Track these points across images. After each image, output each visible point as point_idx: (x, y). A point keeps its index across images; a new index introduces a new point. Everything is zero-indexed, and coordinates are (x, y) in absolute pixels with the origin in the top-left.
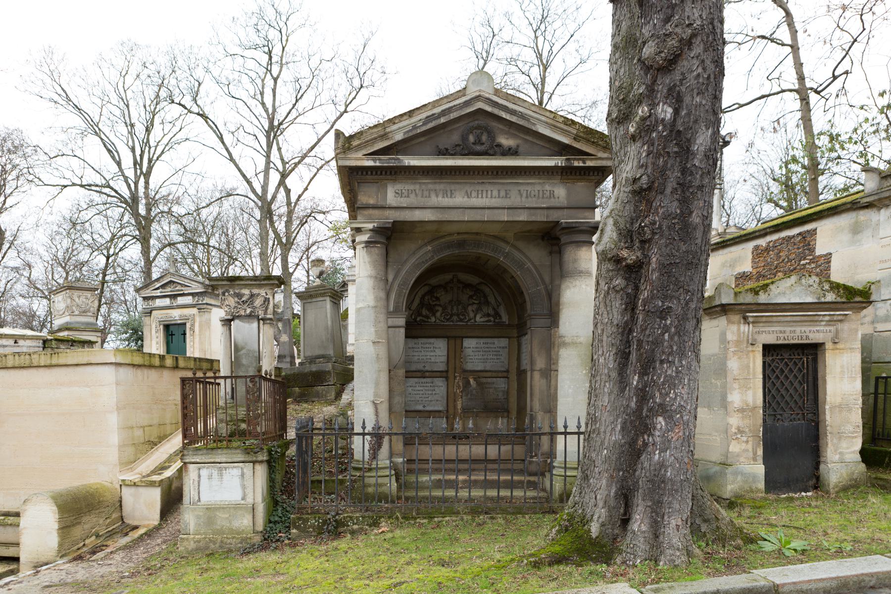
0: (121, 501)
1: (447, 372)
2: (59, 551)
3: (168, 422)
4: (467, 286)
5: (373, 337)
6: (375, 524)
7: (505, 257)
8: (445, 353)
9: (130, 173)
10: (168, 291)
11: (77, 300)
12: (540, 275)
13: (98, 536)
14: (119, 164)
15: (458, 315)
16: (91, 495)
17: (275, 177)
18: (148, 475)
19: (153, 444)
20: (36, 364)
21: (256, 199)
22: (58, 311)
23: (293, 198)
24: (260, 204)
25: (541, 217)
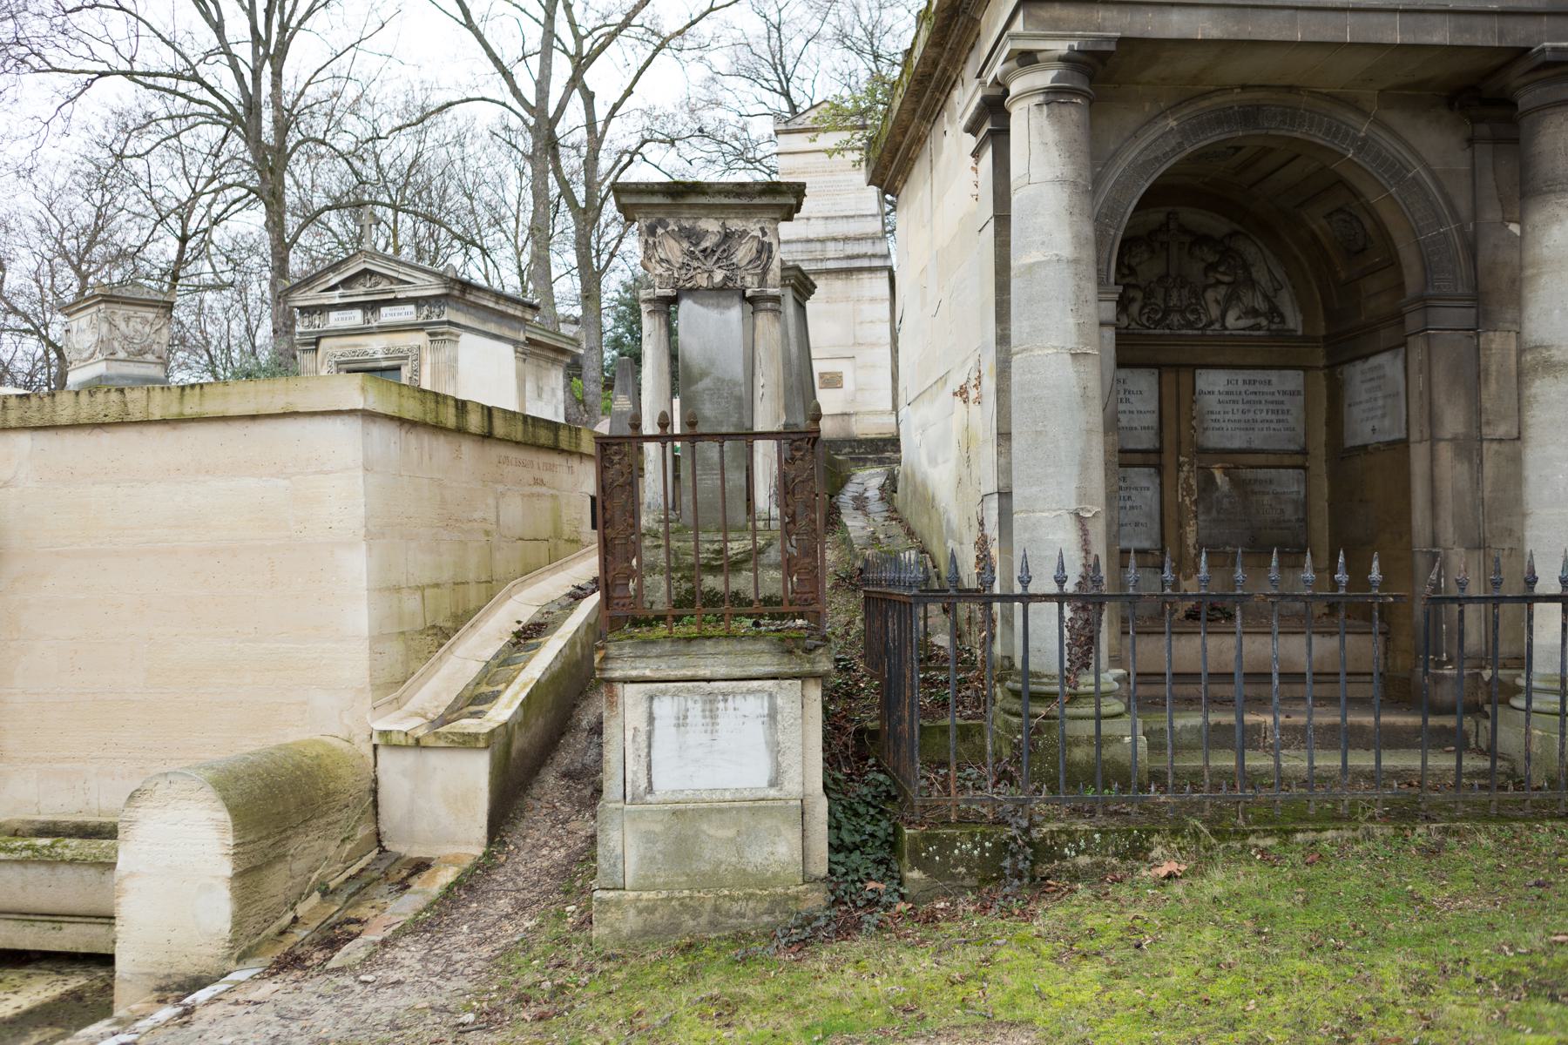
0: (375, 792)
1: (1159, 451)
2: (234, 941)
3: (471, 576)
4: (1202, 239)
5: (1072, 341)
6: (1138, 852)
7: (1360, 150)
8: (1154, 405)
9: (244, 52)
10: (359, 292)
11: (122, 326)
12: (1445, 196)
13: (326, 893)
14: (218, 28)
15: (1182, 312)
16: (308, 774)
17: (562, 68)
18: (444, 720)
19: (442, 633)
20: (138, 416)
22: (79, 352)
23: (601, 113)
24: (532, 121)
25: (1484, 35)
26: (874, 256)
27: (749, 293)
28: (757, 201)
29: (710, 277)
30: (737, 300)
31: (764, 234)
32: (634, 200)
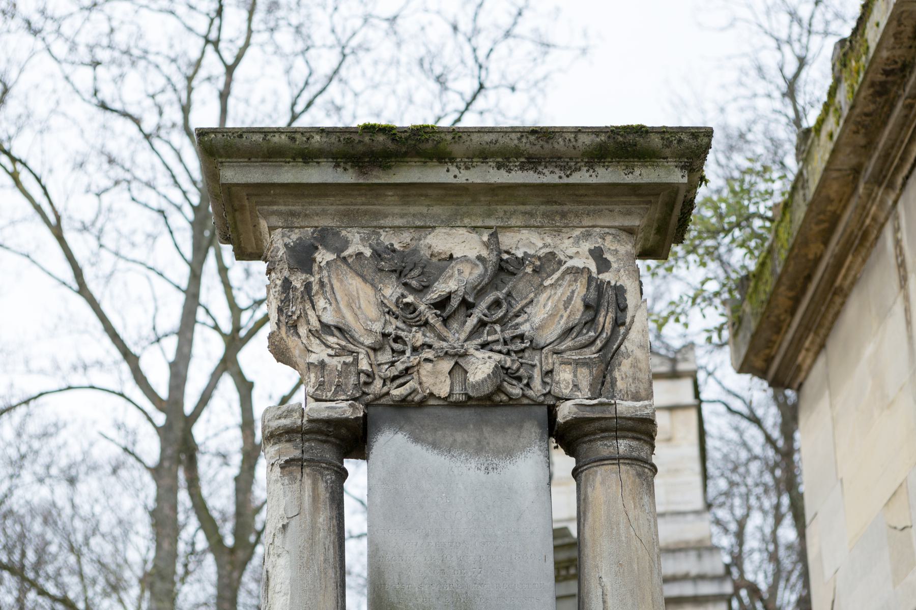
17: (208, 348)
21: (149, 406)
26: (701, 578)
27: (565, 411)
28: (582, 177)
29: (458, 369)
30: (532, 431)
31: (603, 265)
32: (256, 175)
